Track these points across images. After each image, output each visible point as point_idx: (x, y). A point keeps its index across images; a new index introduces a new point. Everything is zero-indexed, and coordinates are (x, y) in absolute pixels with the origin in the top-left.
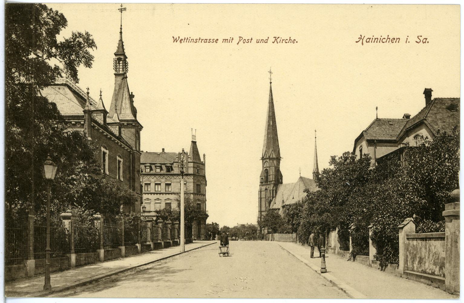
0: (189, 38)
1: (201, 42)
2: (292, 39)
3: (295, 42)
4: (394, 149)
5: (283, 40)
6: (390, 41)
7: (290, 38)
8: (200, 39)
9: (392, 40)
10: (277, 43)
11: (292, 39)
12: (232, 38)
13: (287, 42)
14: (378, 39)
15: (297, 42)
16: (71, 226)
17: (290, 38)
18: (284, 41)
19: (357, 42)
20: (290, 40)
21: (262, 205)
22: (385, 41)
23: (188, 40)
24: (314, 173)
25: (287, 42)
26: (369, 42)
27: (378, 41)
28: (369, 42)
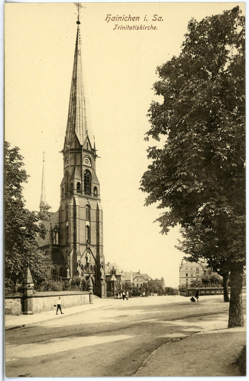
0: (135, 26)
1: (118, 29)
2: (154, 26)
3: (156, 29)
4: (185, 336)
5: (146, 27)
6: (153, 28)
7: (152, 25)
8: (129, 27)
9: (154, 28)
10: (142, 29)
11: (154, 26)
12: (128, 26)
13: (149, 29)
14: (124, 27)
15: (157, 29)
16: (61, 264)
17: (152, 25)
18: (146, 28)
19: (114, 29)
20: (151, 27)
21: (77, 295)
22: (150, 29)
23: (135, 28)
24: (99, 195)
25: (149, 29)
26: (131, 29)
27: (125, 29)
28: (131, 29)
